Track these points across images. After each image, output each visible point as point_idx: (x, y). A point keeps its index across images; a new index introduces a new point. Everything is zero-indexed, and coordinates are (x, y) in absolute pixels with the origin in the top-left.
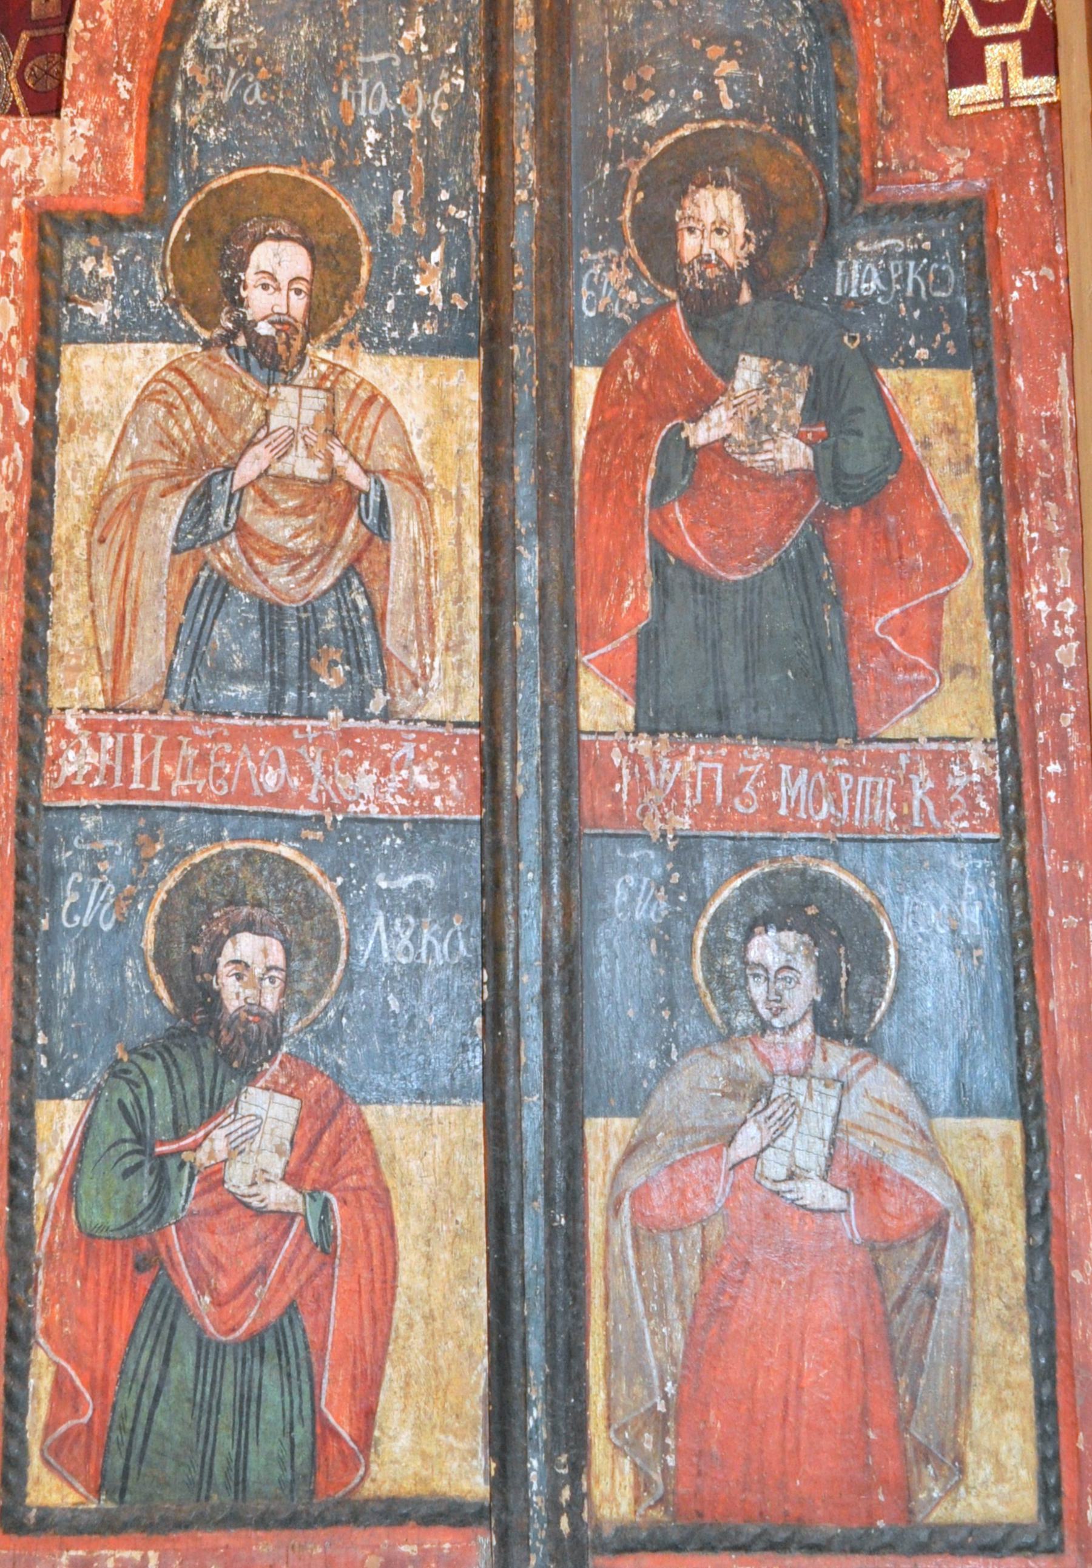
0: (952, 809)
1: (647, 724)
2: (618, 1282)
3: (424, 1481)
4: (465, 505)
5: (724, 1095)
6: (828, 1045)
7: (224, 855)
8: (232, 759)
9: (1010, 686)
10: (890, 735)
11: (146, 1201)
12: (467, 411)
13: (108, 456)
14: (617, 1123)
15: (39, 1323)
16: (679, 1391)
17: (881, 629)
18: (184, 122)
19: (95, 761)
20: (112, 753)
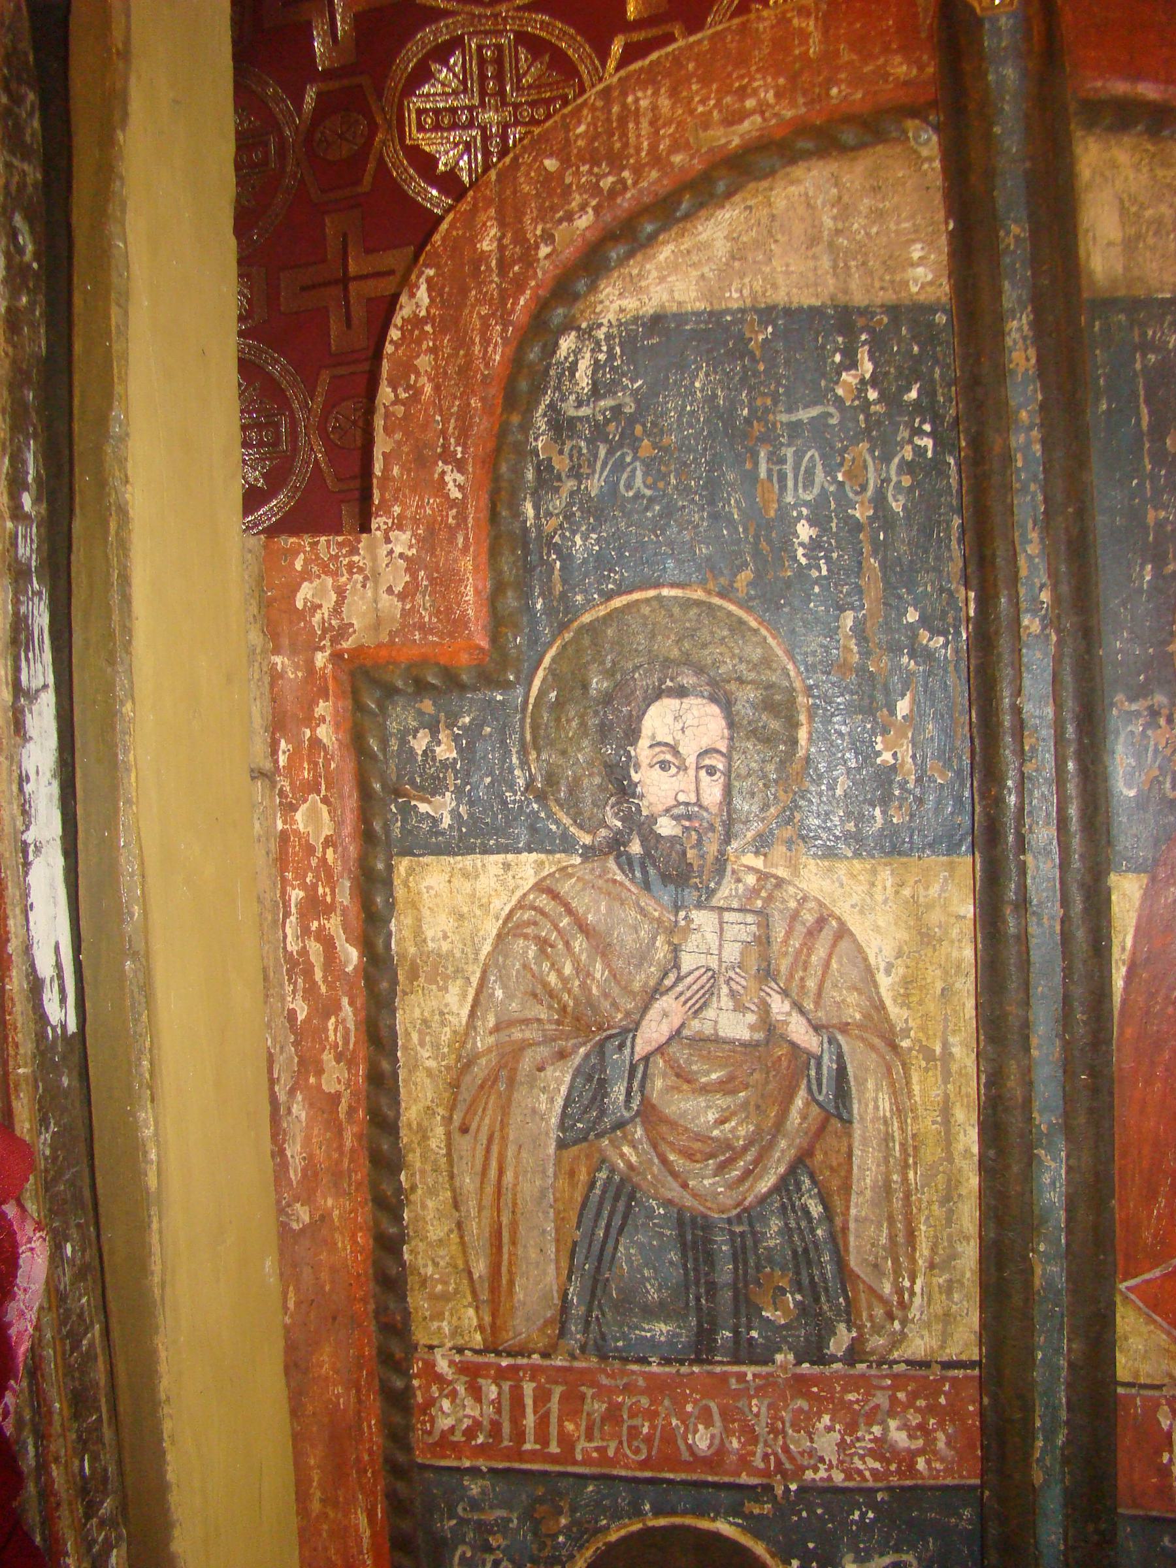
4: (954, 1068)
8: (652, 1415)
12: (954, 933)
13: (465, 1012)
18: (539, 527)
19: (476, 1413)
20: (497, 1404)
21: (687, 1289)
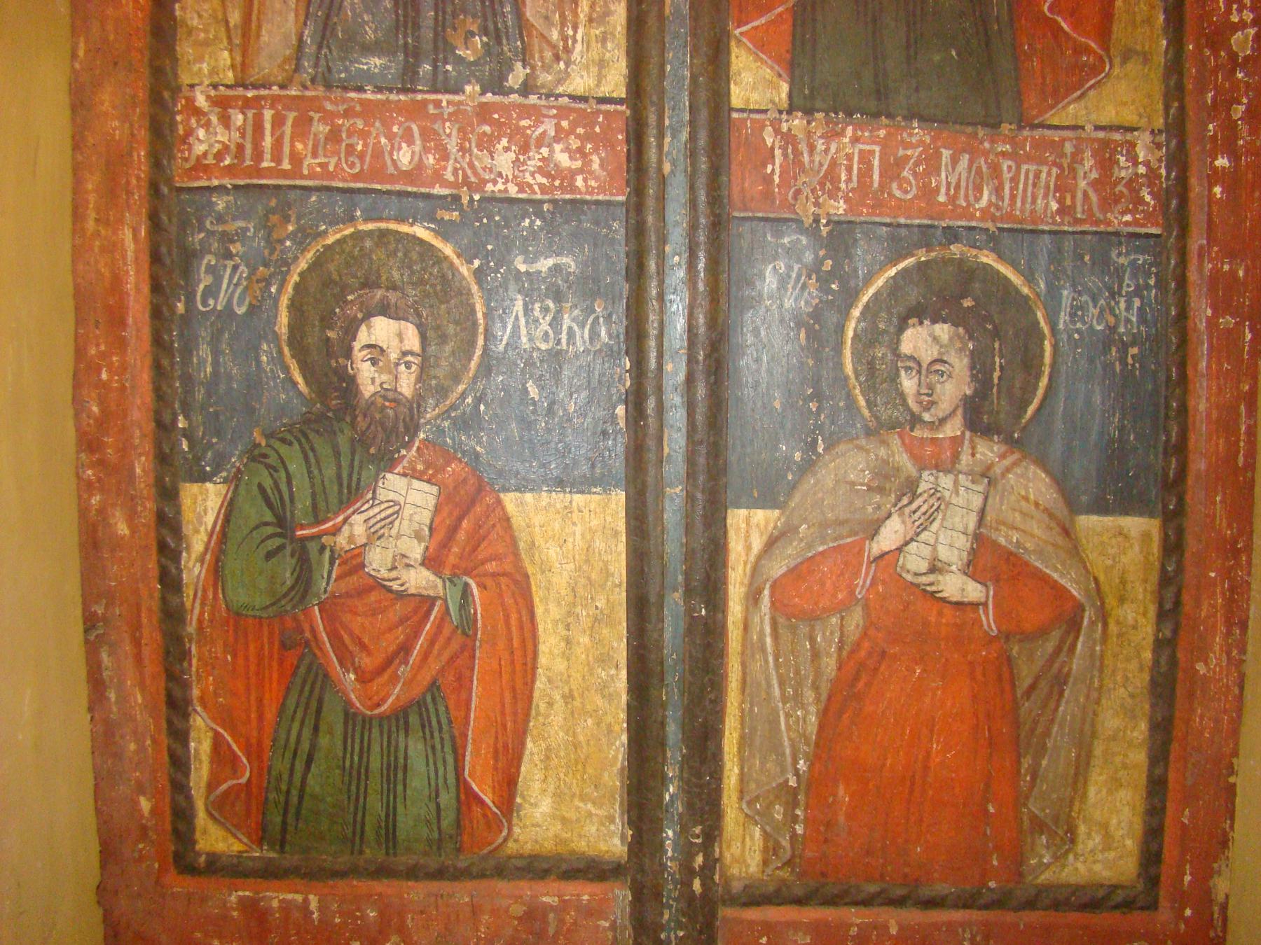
0: (1117, 201)
1: (801, 103)
2: (756, 666)
3: (564, 842)
5: (870, 489)
6: (977, 440)
7: (358, 236)
8: (364, 135)
9: (1181, 75)
10: (1056, 122)
11: (289, 583)
14: (760, 515)
15: (196, 692)
16: (811, 766)
17: (1050, 9)
19: (225, 139)
21: (397, 28)
